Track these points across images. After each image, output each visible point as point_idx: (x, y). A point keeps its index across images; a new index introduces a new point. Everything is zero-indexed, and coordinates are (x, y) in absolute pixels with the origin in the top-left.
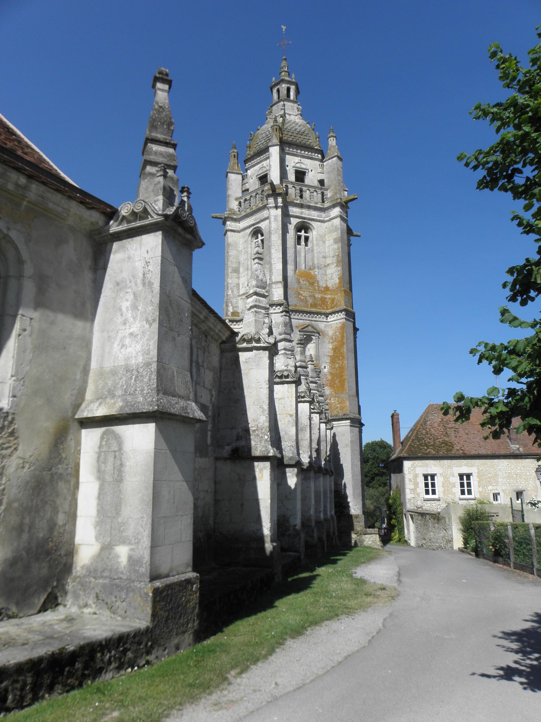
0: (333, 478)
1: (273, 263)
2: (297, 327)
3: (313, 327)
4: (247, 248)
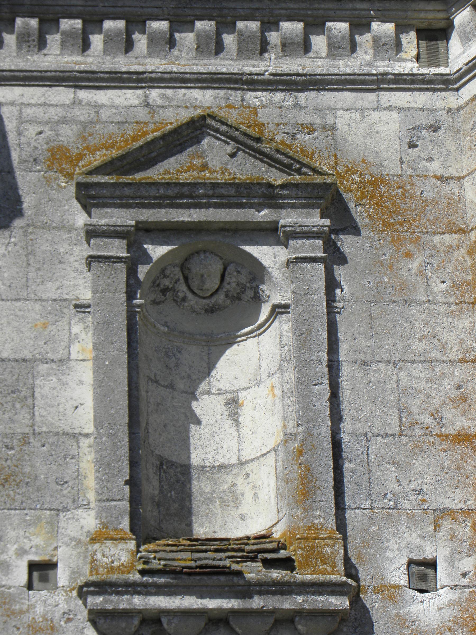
2: (58, 158)
3: (248, 142)
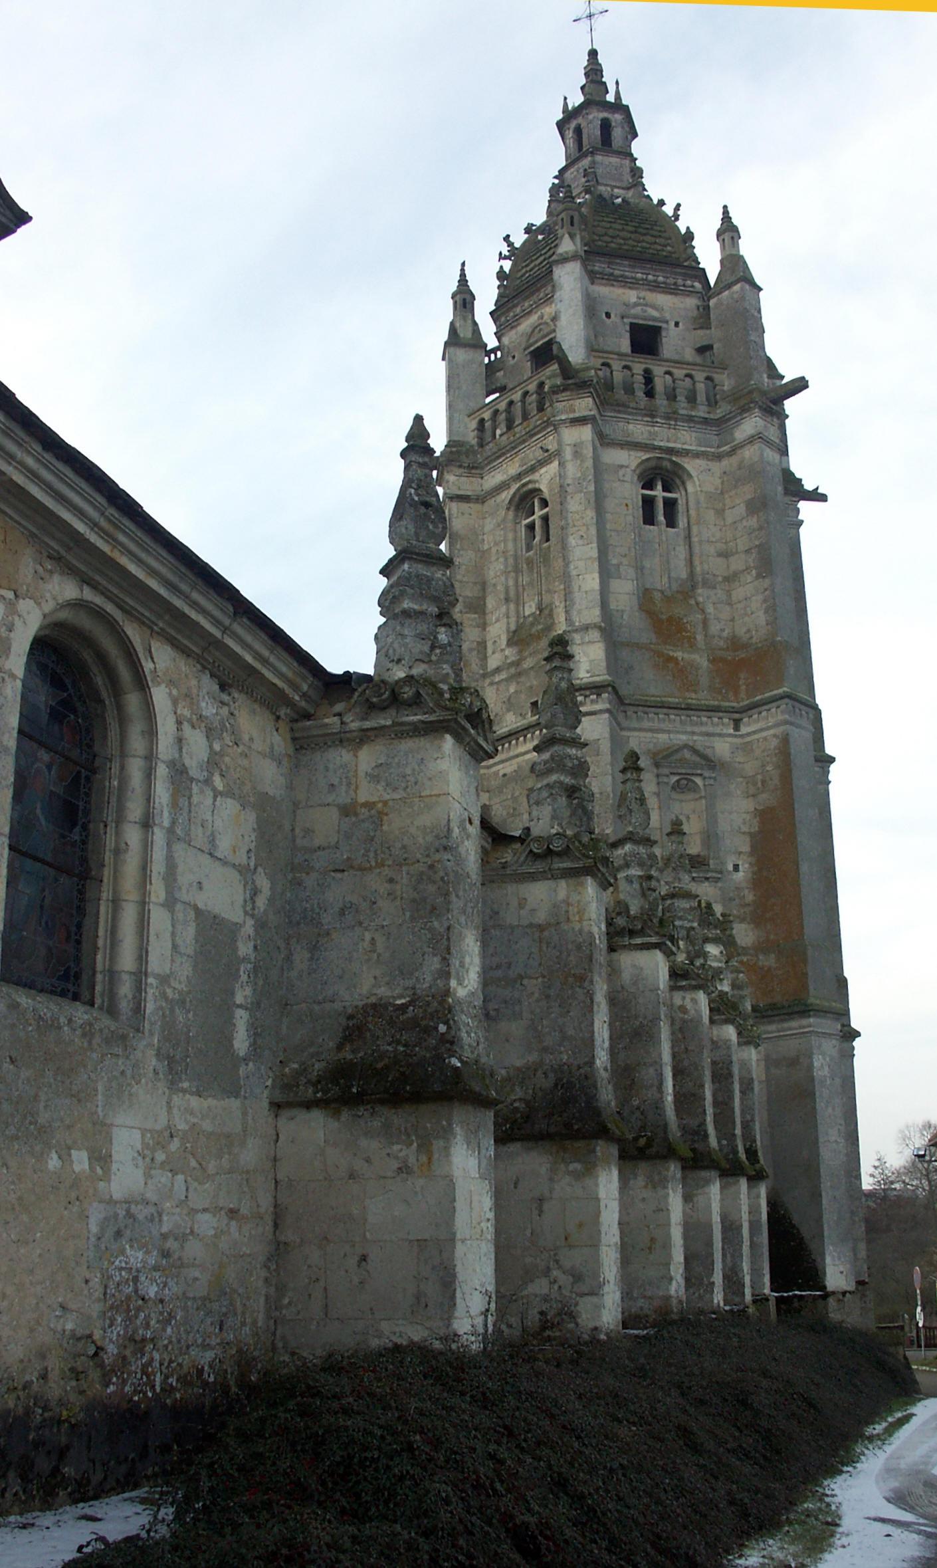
0: (763, 1190)
1: (574, 573)
3: (695, 751)
4: (505, 541)
